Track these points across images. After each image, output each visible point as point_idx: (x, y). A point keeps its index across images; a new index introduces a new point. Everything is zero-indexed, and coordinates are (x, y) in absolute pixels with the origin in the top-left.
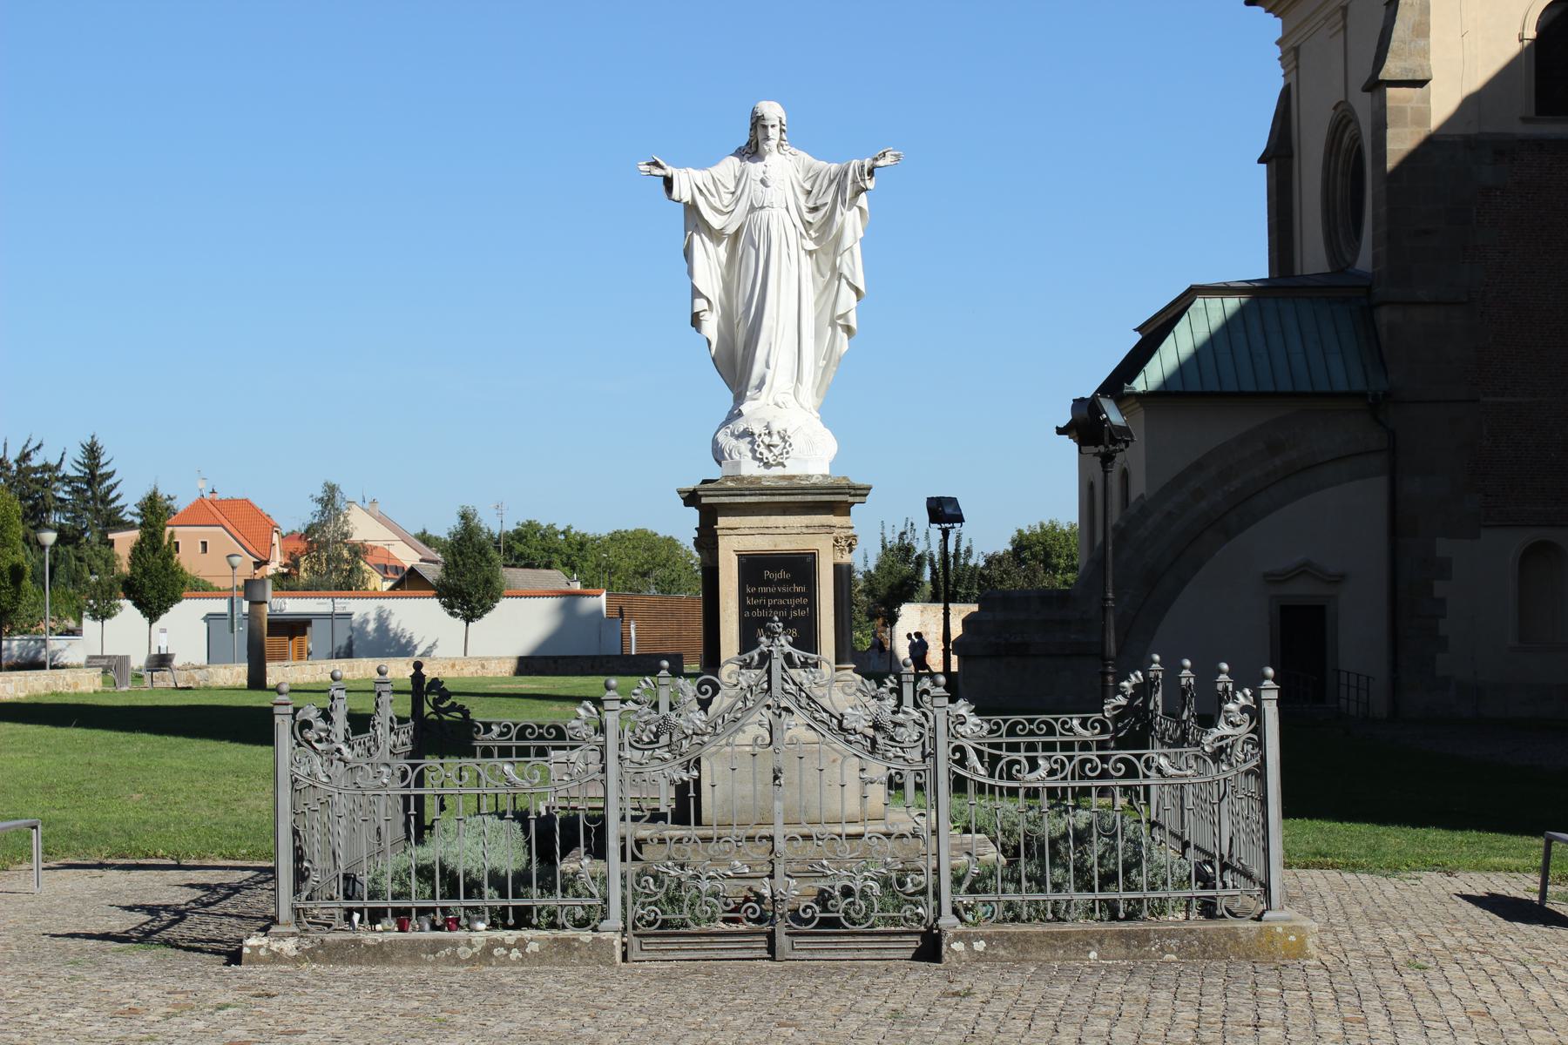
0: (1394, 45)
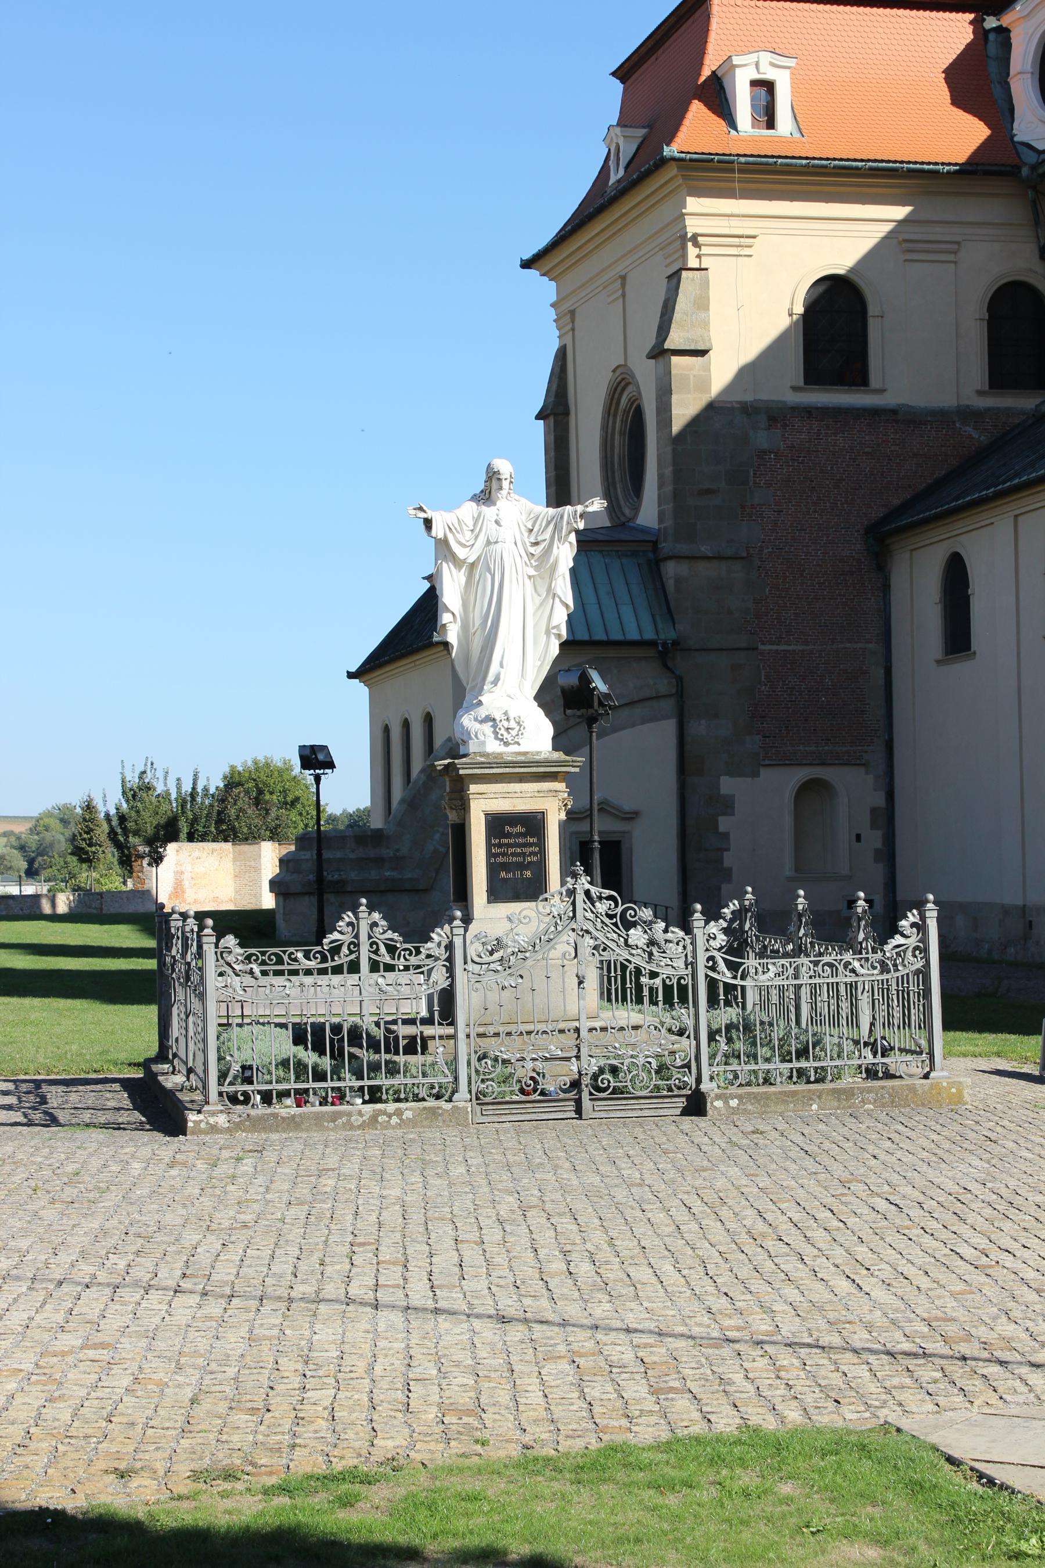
0: (677, 316)
